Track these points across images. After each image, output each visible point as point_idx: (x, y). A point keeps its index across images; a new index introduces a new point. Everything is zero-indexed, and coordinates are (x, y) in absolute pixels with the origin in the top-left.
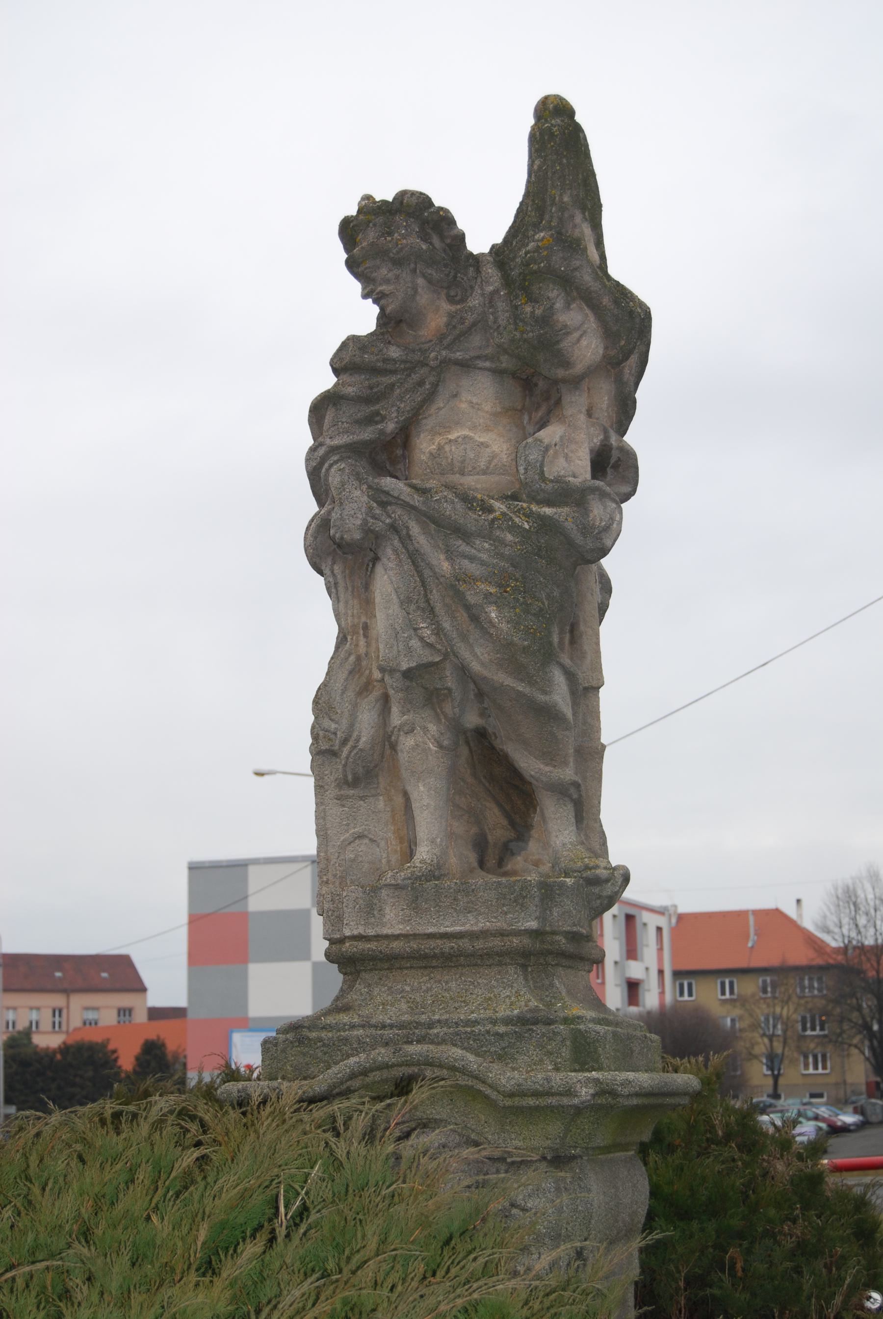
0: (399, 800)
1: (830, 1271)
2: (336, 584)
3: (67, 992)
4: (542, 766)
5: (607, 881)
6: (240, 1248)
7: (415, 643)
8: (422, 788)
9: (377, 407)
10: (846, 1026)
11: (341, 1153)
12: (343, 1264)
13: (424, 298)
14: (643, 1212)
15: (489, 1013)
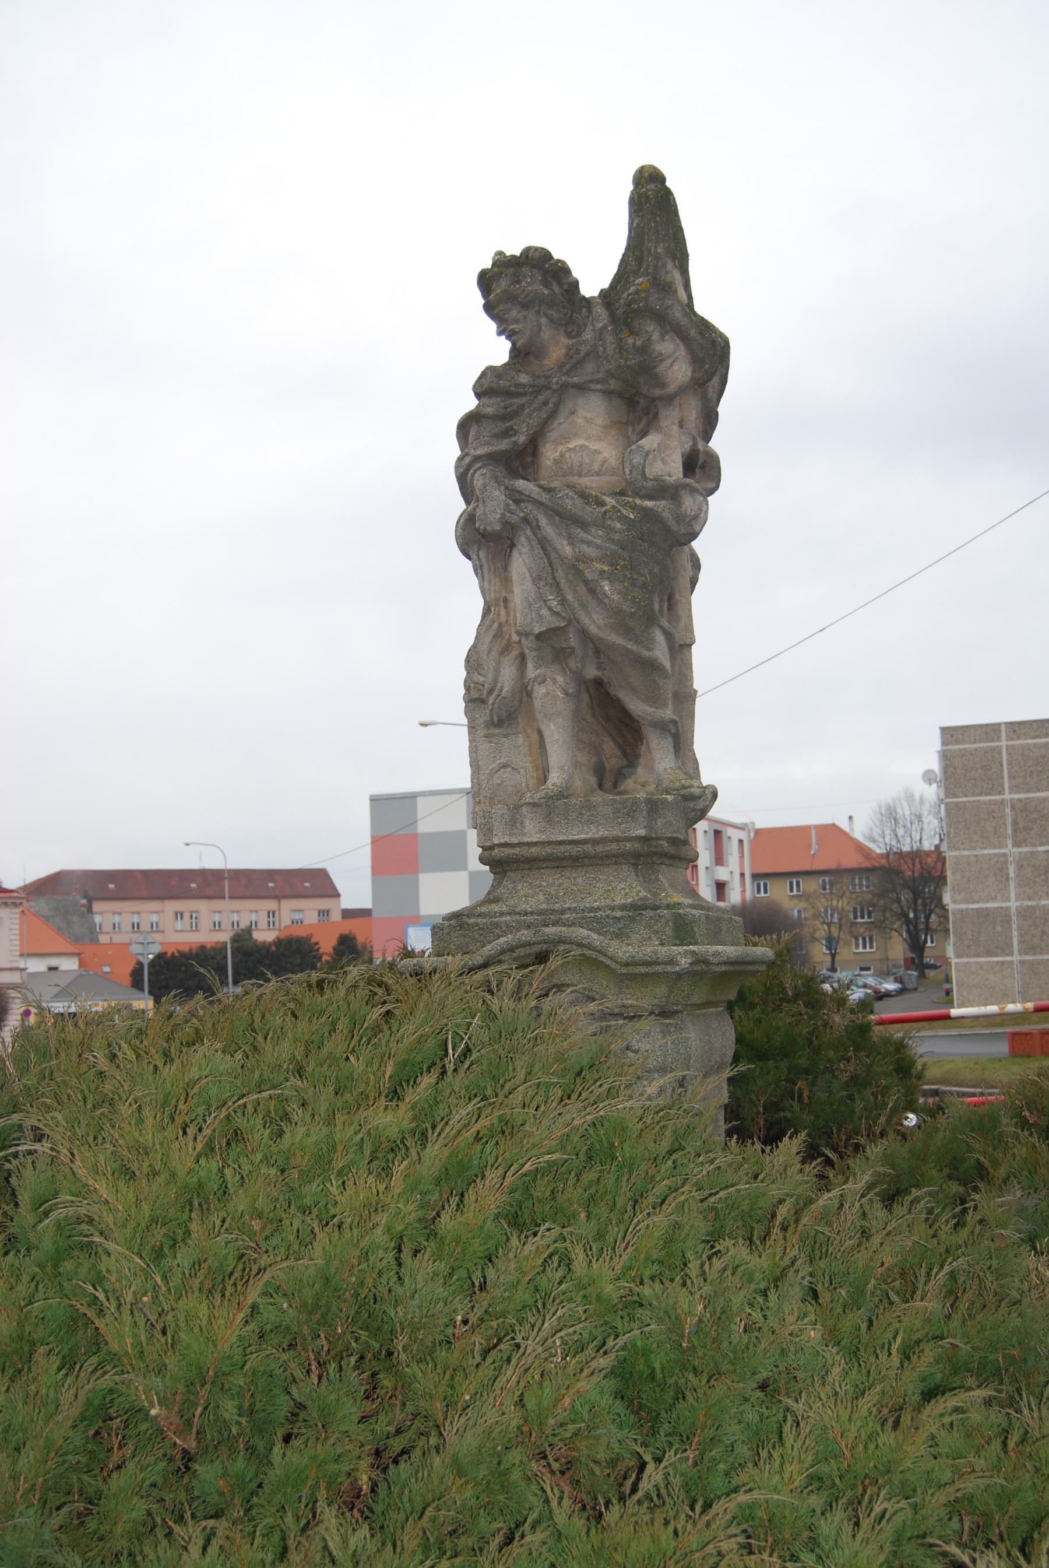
0: (535, 736)
1: (877, 1098)
2: (481, 566)
3: (278, 898)
4: (647, 708)
5: (700, 797)
6: (419, 1079)
7: (545, 612)
8: (552, 727)
9: (510, 423)
10: (888, 915)
11: (495, 1008)
12: (498, 1090)
13: (547, 334)
14: (730, 1054)
15: (608, 902)
